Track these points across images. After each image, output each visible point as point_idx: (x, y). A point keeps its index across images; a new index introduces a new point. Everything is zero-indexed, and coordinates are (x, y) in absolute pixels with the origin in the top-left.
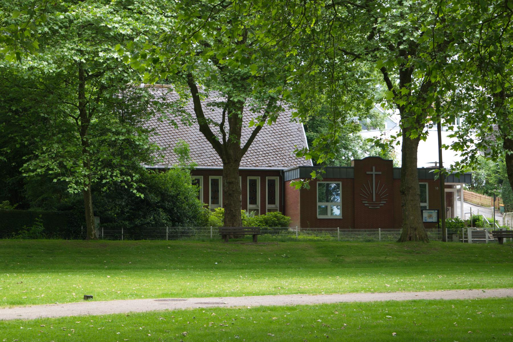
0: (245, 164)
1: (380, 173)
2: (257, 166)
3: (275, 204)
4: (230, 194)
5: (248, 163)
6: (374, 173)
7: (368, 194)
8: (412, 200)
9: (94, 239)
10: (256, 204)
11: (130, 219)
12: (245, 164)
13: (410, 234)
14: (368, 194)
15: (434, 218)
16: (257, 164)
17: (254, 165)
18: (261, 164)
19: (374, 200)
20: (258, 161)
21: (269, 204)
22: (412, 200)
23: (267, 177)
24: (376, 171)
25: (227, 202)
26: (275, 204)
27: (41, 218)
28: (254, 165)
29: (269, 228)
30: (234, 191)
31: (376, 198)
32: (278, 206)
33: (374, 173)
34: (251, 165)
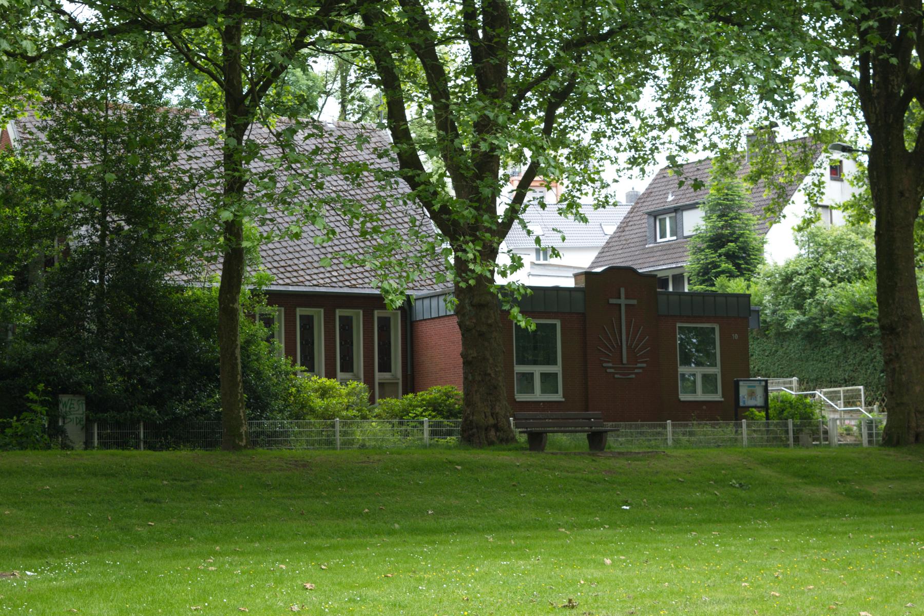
0: (328, 280)
1: (634, 302)
2: (354, 286)
3: (390, 371)
4: (481, 334)
5: (334, 279)
6: (623, 301)
7: (613, 347)
8: (915, 348)
9: (245, 447)
10: (352, 371)
11: (157, 401)
12: (328, 280)
13: (918, 427)
14: (613, 347)
15: (758, 398)
16: (353, 282)
17: (347, 283)
18: (360, 281)
19: (625, 361)
20: (353, 276)
21: (380, 371)
22: (915, 348)
23: (376, 312)
24: (626, 298)
25: (473, 353)
26: (390, 371)
27: (45, 392)
28: (347, 283)
29: (446, 422)
30: (490, 325)
31: (628, 358)
32: (399, 375)
33: (623, 301)
34: (341, 284)
